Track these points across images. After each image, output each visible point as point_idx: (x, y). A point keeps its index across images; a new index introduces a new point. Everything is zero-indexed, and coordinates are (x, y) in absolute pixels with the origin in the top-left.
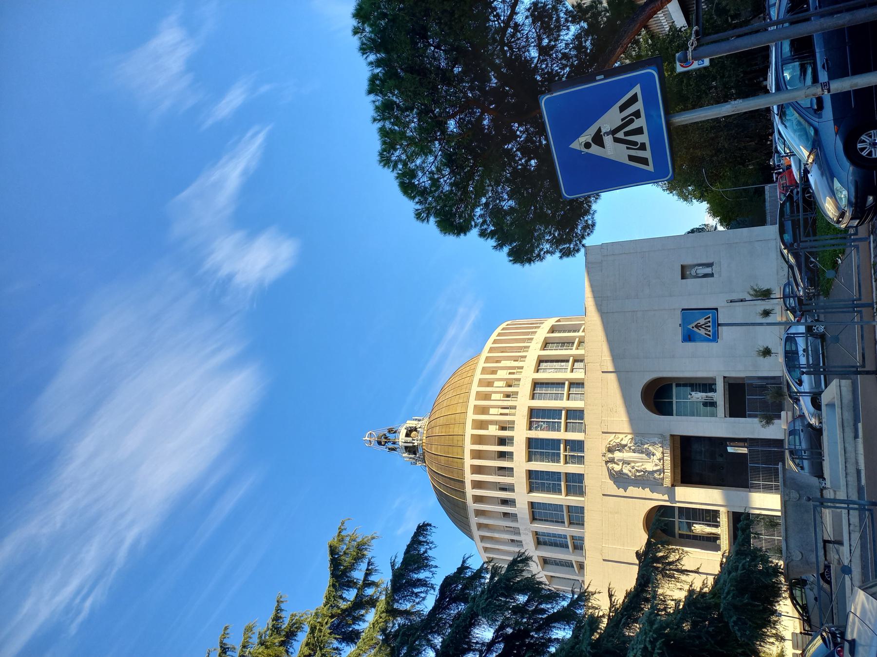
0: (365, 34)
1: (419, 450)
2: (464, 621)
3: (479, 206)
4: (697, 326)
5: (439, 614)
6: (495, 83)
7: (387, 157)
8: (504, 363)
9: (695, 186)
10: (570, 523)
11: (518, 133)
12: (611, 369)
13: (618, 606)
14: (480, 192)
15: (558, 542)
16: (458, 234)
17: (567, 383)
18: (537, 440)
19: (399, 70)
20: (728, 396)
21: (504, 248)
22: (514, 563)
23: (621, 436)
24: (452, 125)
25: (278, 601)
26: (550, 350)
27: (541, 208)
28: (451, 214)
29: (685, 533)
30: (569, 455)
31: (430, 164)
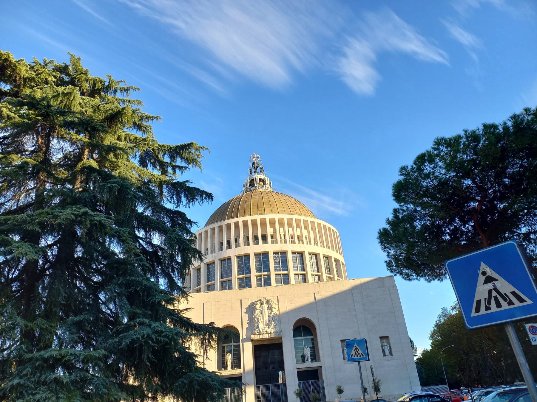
0: (526, 116)
2: (162, 227)
3: (414, 206)
4: (356, 349)
5: (163, 211)
6: (500, 206)
7: (441, 143)
8: (312, 233)
9: (442, 341)
10: (222, 282)
11: (467, 226)
12: (317, 298)
13: (181, 314)
14: (424, 206)
15: (210, 276)
16: (394, 195)
18: (268, 258)
20: (310, 369)
21: (388, 225)
22: (199, 252)
24: (468, 182)
25: (157, 117)
26: (324, 260)
27: (418, 246)
29: (225, 350)
30: (261, 278)
31: (440, 171)
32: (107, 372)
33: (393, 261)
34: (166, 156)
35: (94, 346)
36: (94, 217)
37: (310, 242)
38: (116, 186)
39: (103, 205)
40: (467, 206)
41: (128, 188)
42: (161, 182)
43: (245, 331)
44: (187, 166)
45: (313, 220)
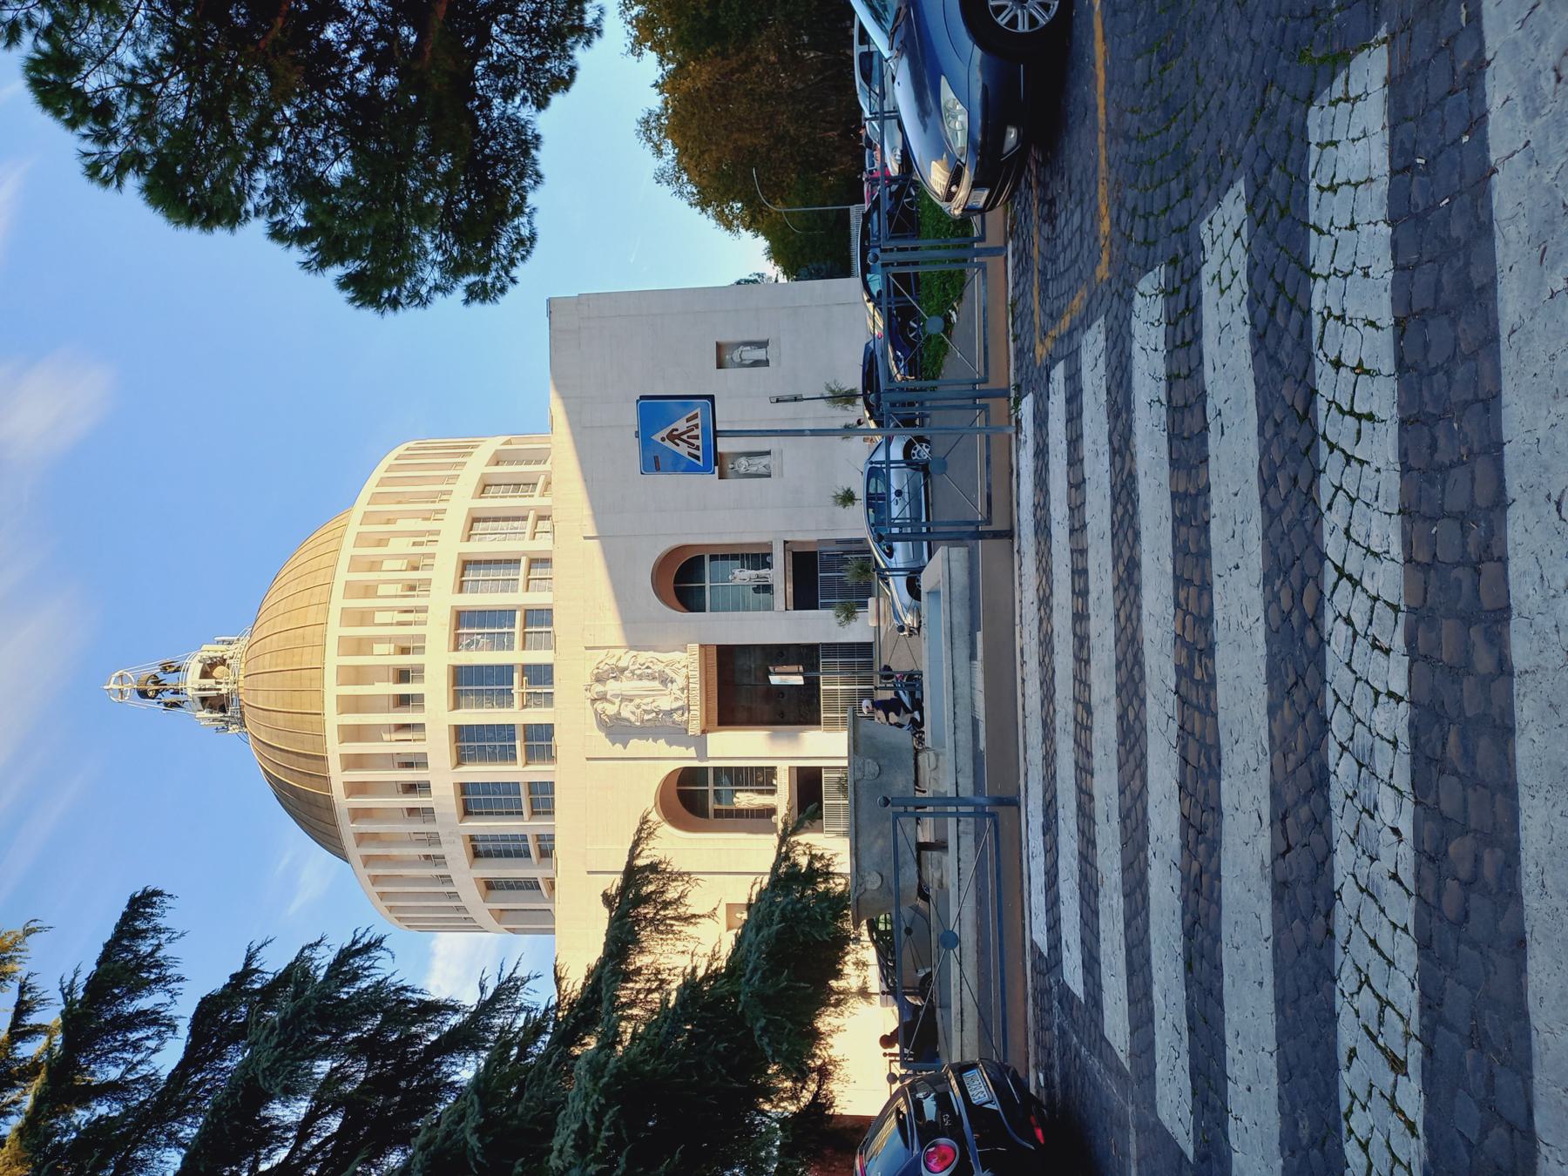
4: (672, 437)
8: (402, 525)
12: (592, 533)
15: (513, 849)
37: (430, 533)
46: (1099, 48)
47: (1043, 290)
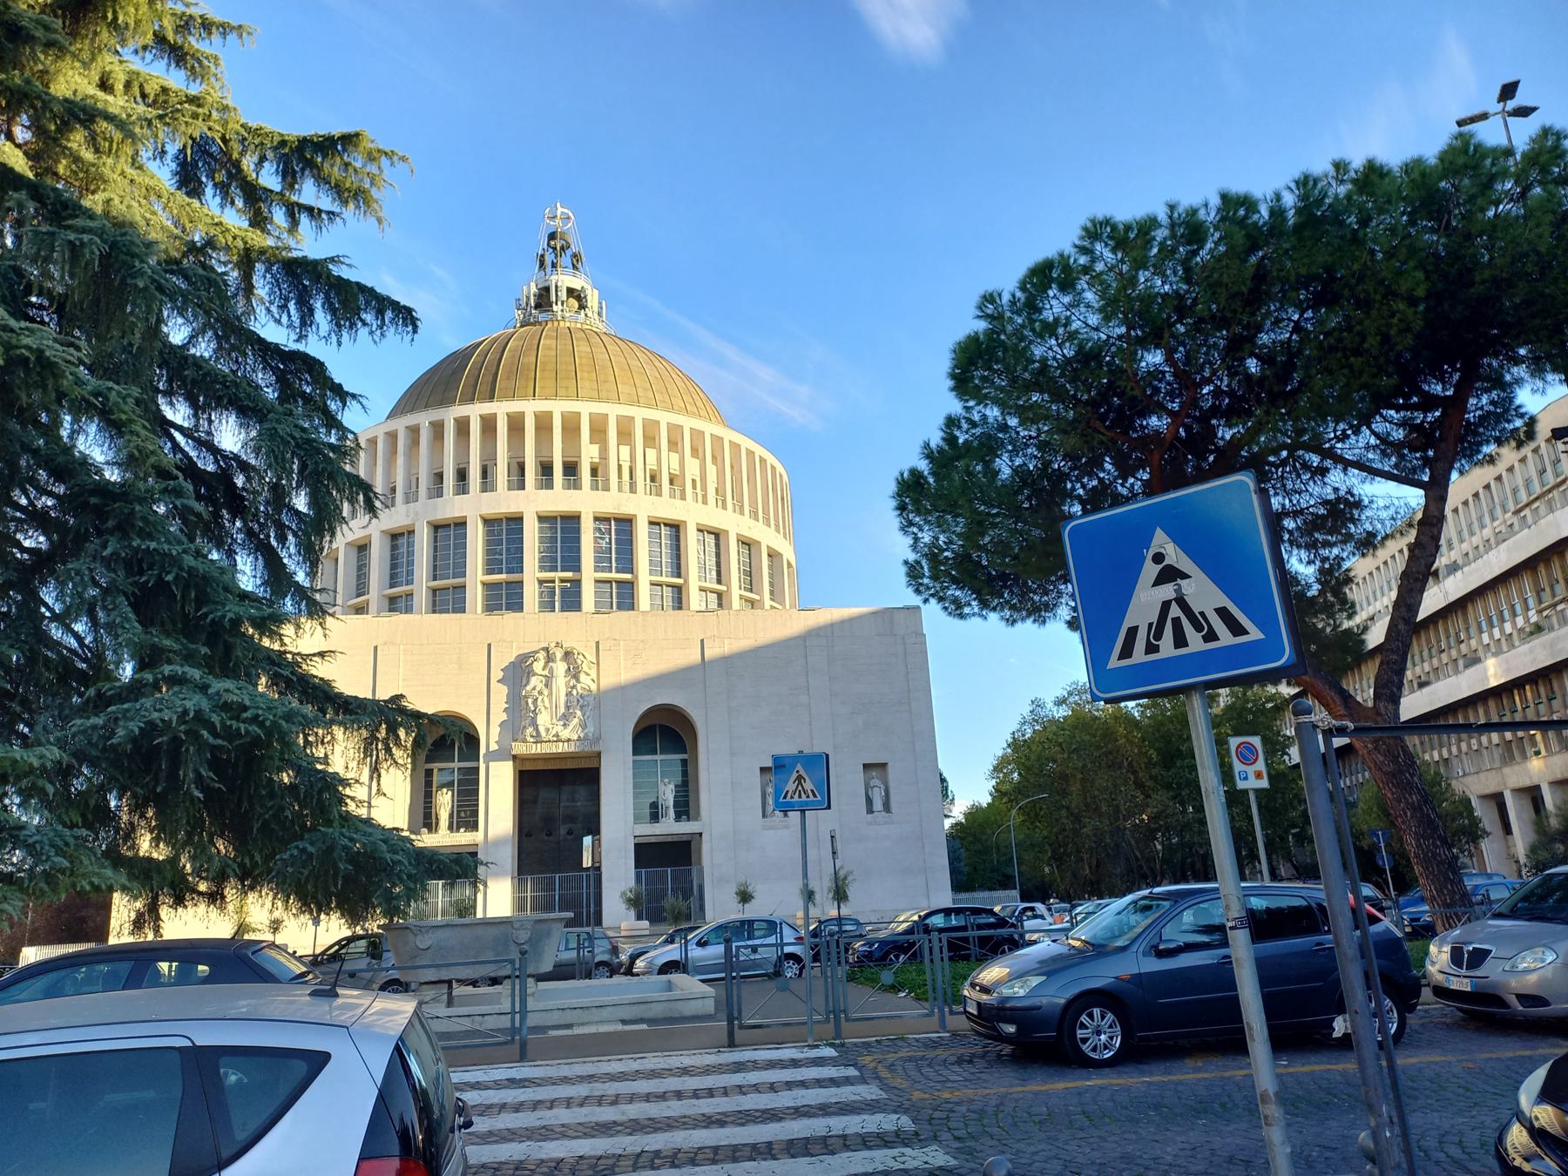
1: (544, 315)
3: (1002, 413)
4: (800, 778)
5: (253, 349)
8: (711, 470)
10: (434, 591)
11: (1131, 480)
13: (304, 667)
14: (1029, 415)
15: (399, 569)
16: (953, 376)
17: (679, 581)
18: (578, 531)
19: (1260, 254)
22: (366, 488)
23: (594, 674)
24: (1154, 358)
25: (240, 27)
27: (994, 525)
28: (990, 360)
32: (67, 813)
33: (924, 563)
34: (269, 168)
35: (23, 737)
36: (18, 335)
37: (705, 497)
38: (96, 243)
39: (51, 306)
40: (1141, 426)
41: (134, 255)
42: (248, 250)
43: (495, 731)
44: (337, 209)
45: (720, 431)
46: (1061, 1085)
47: (910, 1059)
